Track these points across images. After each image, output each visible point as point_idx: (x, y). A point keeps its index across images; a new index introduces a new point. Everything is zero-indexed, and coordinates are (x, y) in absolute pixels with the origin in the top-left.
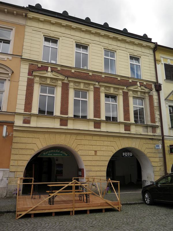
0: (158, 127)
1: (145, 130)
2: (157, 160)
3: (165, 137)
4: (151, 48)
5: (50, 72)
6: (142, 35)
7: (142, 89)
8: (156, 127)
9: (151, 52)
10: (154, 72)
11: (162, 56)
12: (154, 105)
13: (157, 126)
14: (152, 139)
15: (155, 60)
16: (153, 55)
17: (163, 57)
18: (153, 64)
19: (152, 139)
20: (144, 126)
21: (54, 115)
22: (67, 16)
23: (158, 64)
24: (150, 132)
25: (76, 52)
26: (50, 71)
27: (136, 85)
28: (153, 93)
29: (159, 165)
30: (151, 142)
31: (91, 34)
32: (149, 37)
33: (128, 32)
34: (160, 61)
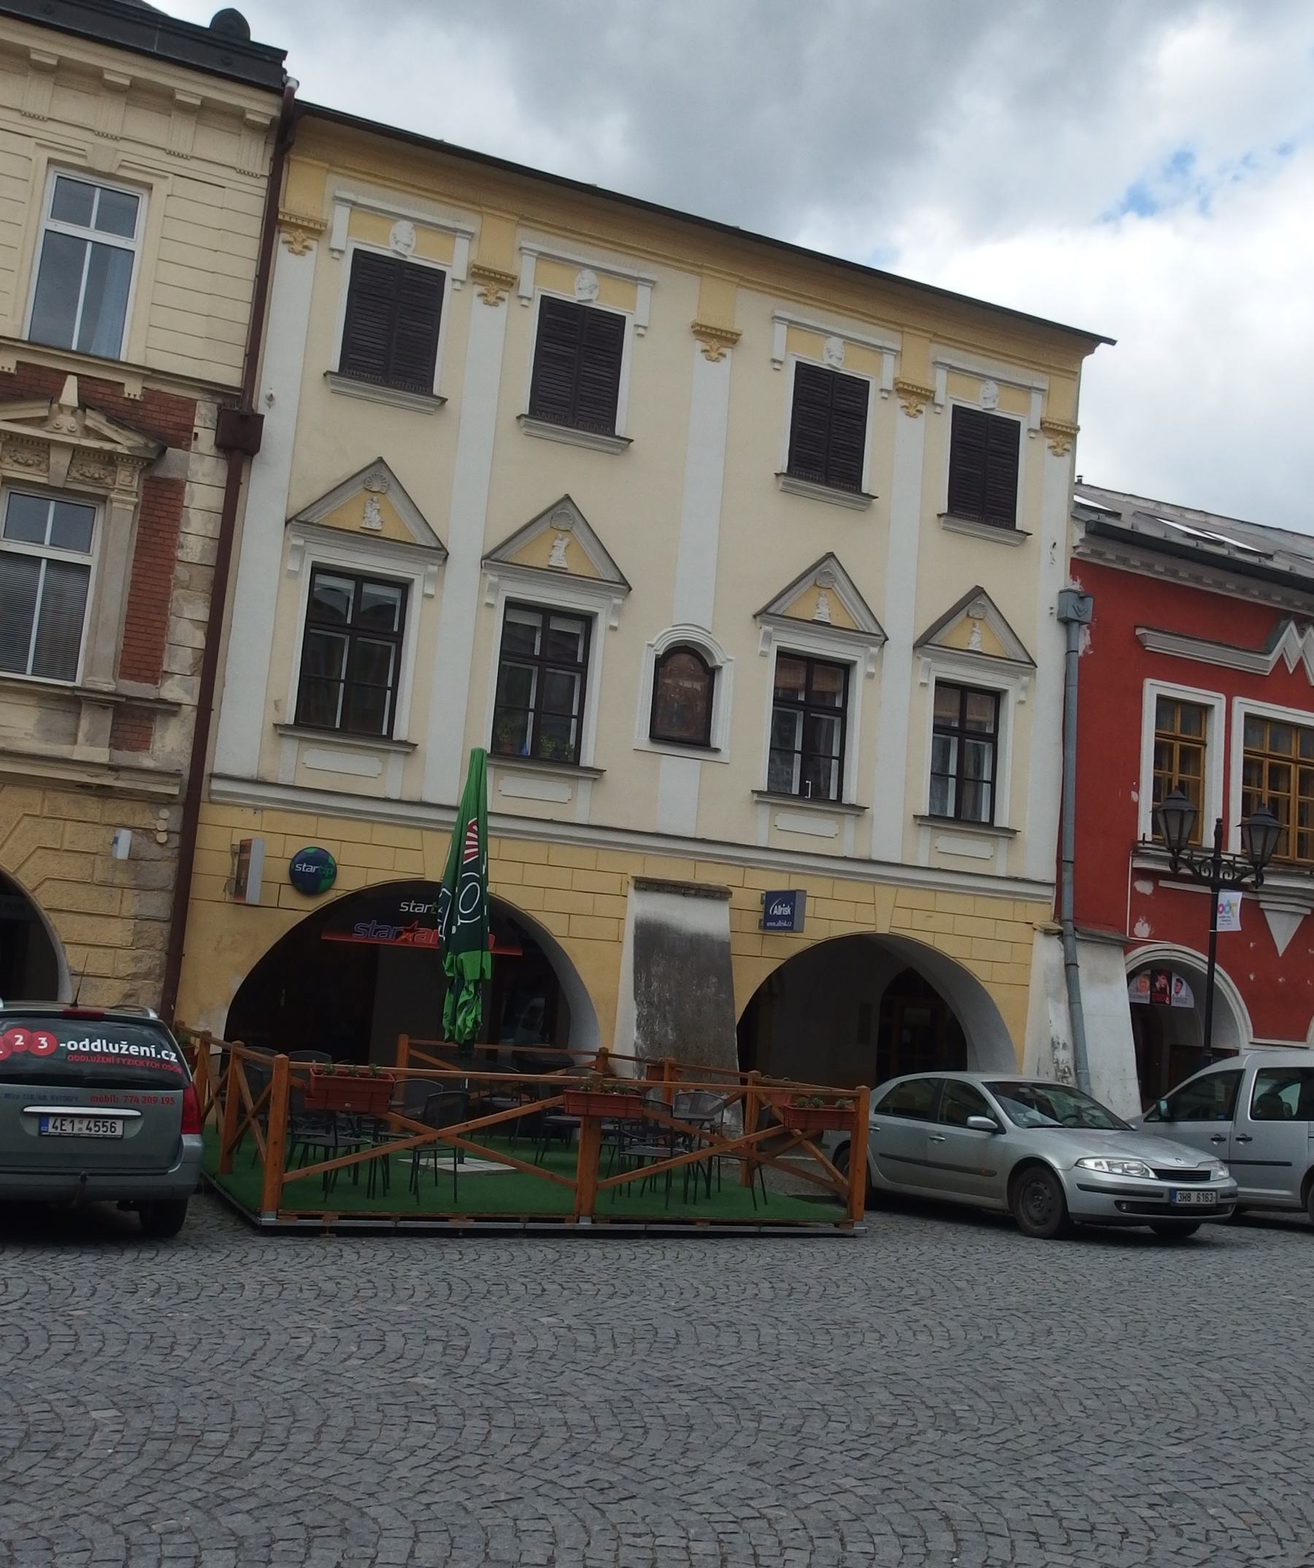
0: (175, 714)
1: (61, 721)
2: (118, 932)
3: (492, 822)
4: (253, 127)
5: (74, 411)
6: (202, 18)
7: (88, 432)
8: (153, 712)
9: (255, 157)
10: (243, 313)
11: (778, 313)
12: (180, 554)
13: (172, 709)
14: (104, 792)
15: (272, 222)
16: (264, 183)
17: (354, 203)
18: (252, 248)
19: (104, 792)
20: (51, 694)
21: (78, 683)
22: (240, 43)
23: (292, 251)
24: (91, 741)
25: (47, 230)
26: (75, 404)
27: (52, 394)
28: (193, 466)
29: (126, 968)
30: (93, 808)
31: (174, 113)
32: (258, 35)
33: (255, 37)
34: (317, 230)
